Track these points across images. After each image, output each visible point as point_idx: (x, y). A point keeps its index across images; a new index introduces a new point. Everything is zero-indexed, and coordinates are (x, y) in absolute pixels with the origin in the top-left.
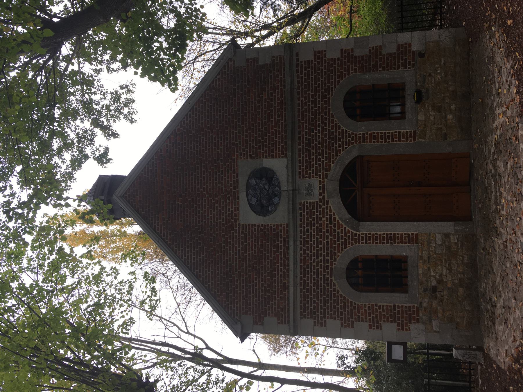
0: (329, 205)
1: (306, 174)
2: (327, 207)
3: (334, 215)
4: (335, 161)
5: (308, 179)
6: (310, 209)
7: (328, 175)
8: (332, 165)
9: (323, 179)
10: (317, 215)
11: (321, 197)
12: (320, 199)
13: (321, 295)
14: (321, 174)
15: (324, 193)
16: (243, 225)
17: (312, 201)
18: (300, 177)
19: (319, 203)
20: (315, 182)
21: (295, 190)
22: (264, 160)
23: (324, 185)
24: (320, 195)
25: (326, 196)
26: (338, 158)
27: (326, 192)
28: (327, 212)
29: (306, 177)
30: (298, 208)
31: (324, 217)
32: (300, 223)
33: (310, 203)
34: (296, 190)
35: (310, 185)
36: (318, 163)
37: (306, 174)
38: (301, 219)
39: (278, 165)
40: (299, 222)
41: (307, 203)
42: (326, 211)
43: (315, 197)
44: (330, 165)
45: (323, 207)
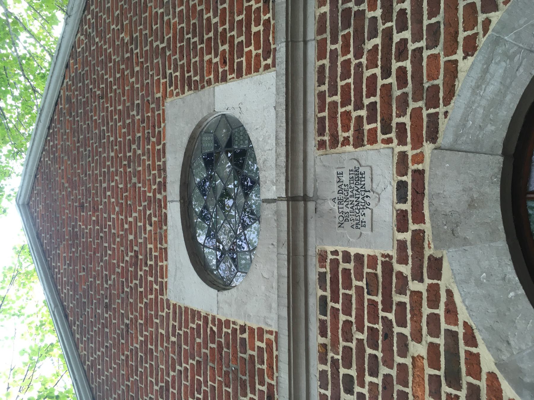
0: (444, 283)
1: (346, 128)
2: (434, 290)
3: (471, 340)
4: (482, 41)
5: (349, 148)
6: (359, 290)
7: (443, 123)
8: (464, 65)
9: (417, 143)
10: (387, 323)
11: (407, 236)
12: (402, 245)
13: (403, 102)
14: (406, 120)
15: (419, 218)
16: (175, 305)
17: (365, 251)
18: (321, 145)
19: (398, 267)
20: (379, 162)
21: (298, 199)
22: (220, 89)
23: (419, 175)
24: (402, 226)
25: (429, 235)
26: (495, 17)
27: (426, 212)
28: (434, 320)
29: (346, 142)
30: (313, 277)
31: (418, 337)
32: (322, 340)
33: (359, 258)
34: (305, 198)
35: (357, 176)
36: (395, 65)
37: (346, 128)
38: (323, 325)
39: (252, 100)
40: (316, 340)
41: (347, 257)
42: (426, 311)
43: (379, 240)
44: (452, 69)
45: (414, 286)
